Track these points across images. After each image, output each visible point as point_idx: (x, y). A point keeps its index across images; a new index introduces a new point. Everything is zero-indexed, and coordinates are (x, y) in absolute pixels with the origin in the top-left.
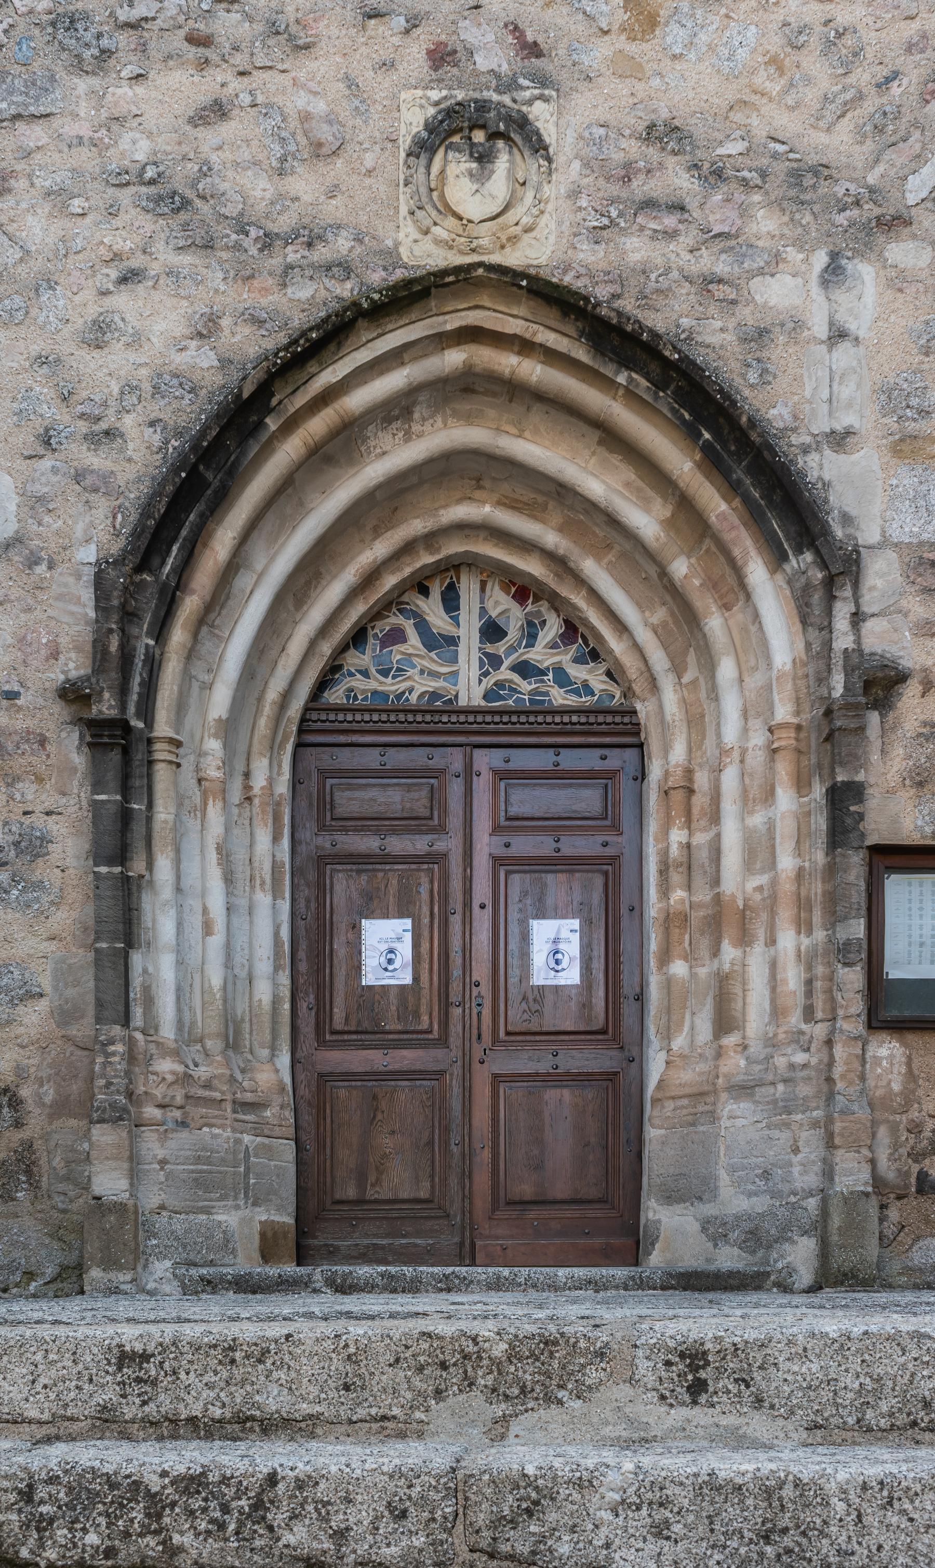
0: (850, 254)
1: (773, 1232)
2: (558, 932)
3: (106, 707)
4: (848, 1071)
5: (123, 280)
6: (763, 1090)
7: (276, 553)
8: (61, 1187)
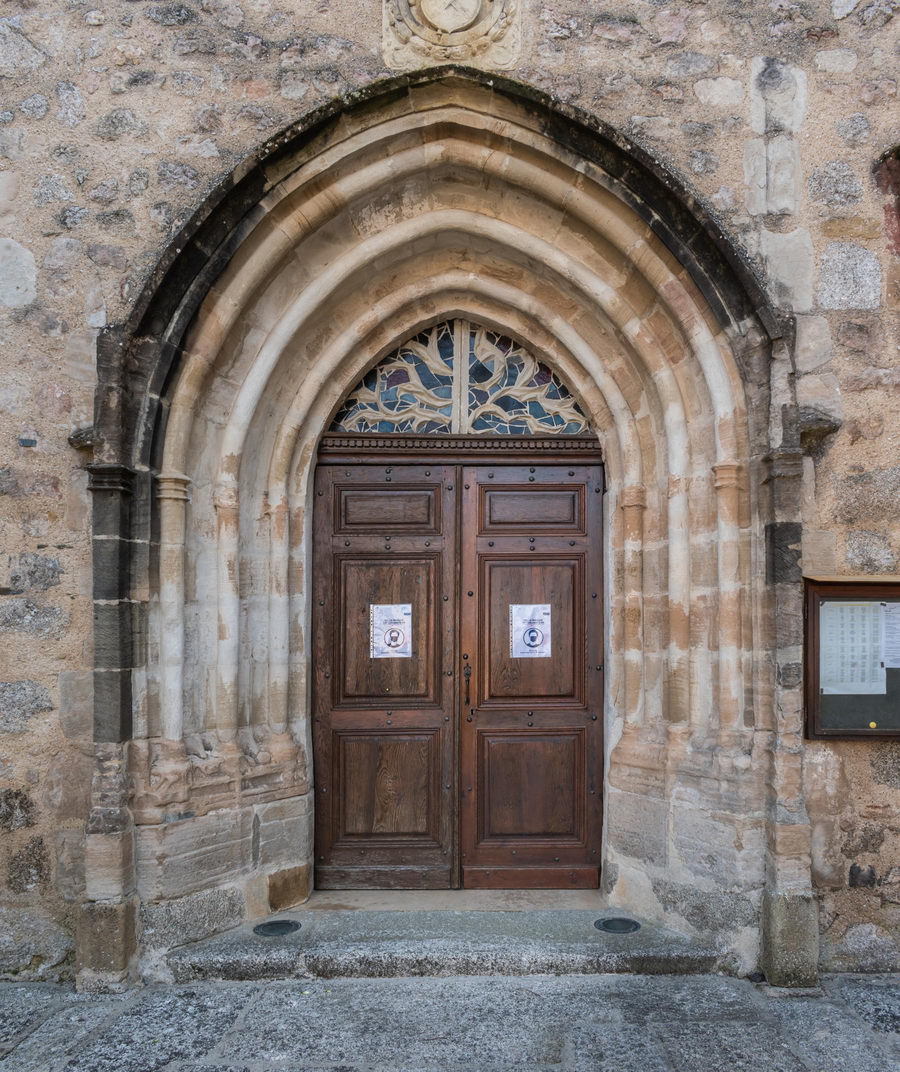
0: (784, 60)
1: (718, 915)
2: (533, 614)
3: (107, 457)
4: (789, 783)
5: (134, 82)
6: (708, 781)
7: (283, 316)
8: (67, 880)
